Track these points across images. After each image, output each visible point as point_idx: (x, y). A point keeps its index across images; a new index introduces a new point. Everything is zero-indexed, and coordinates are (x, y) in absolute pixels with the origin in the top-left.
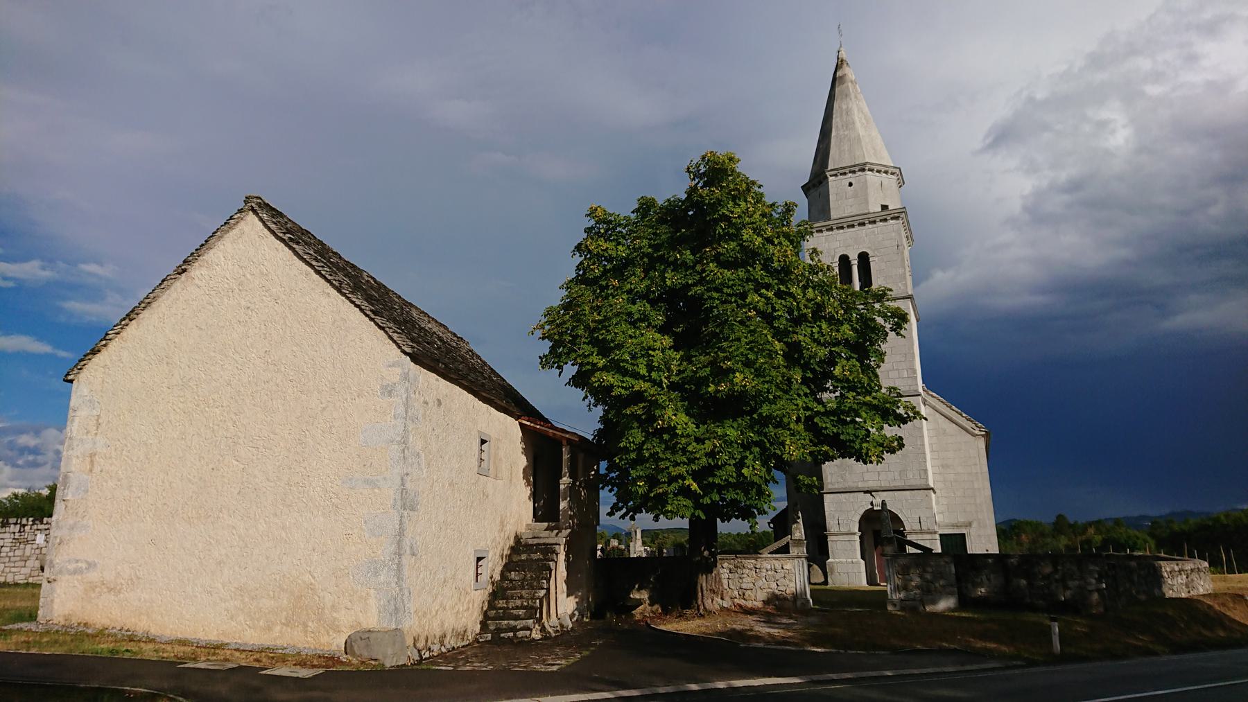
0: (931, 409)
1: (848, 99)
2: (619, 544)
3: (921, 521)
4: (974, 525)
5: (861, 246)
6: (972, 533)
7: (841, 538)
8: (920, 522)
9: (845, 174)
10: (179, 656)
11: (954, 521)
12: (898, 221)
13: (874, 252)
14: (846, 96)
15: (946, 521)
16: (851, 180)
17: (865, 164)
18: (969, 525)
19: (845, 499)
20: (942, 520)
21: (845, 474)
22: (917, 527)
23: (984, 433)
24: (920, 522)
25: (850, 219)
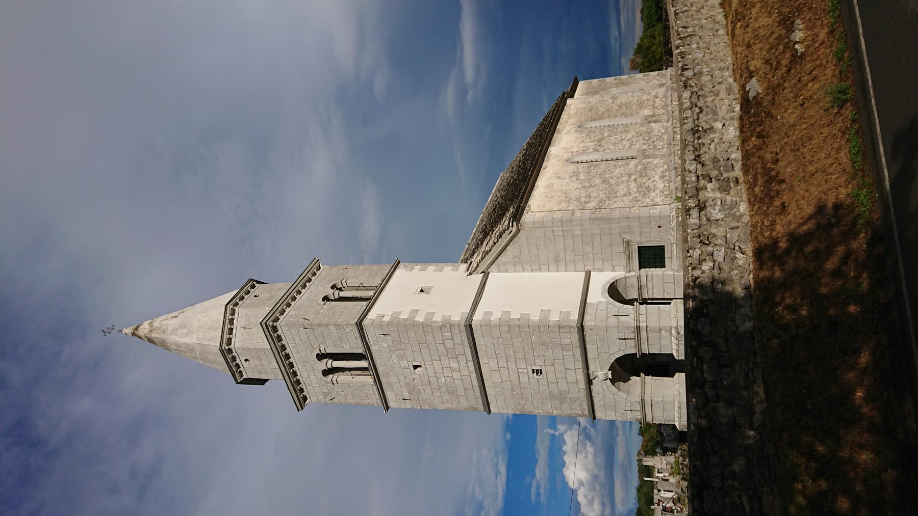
0: (492, 266)
1: (166, 341)
2: (663, 142)
3: (623, 337)
4: (628, 237)
5: (311, 358)
6: (638, 239)
7: (648, 392)
8: (625, 339)
9: (238, 366)
10: (722, 10)
11: (623, 256)
12: (278, 327)
13: (316, 348)
14: (163, 342)
15: (623, 263)
16: (243, 361)
17: (221, 350)
18: (627, 243)
19: (600, 401)
20: (622, 267)
21: (570, 398)
22: (632, 343)
23: (515, 223)
24: (625, 339)
25: (283, 369)
